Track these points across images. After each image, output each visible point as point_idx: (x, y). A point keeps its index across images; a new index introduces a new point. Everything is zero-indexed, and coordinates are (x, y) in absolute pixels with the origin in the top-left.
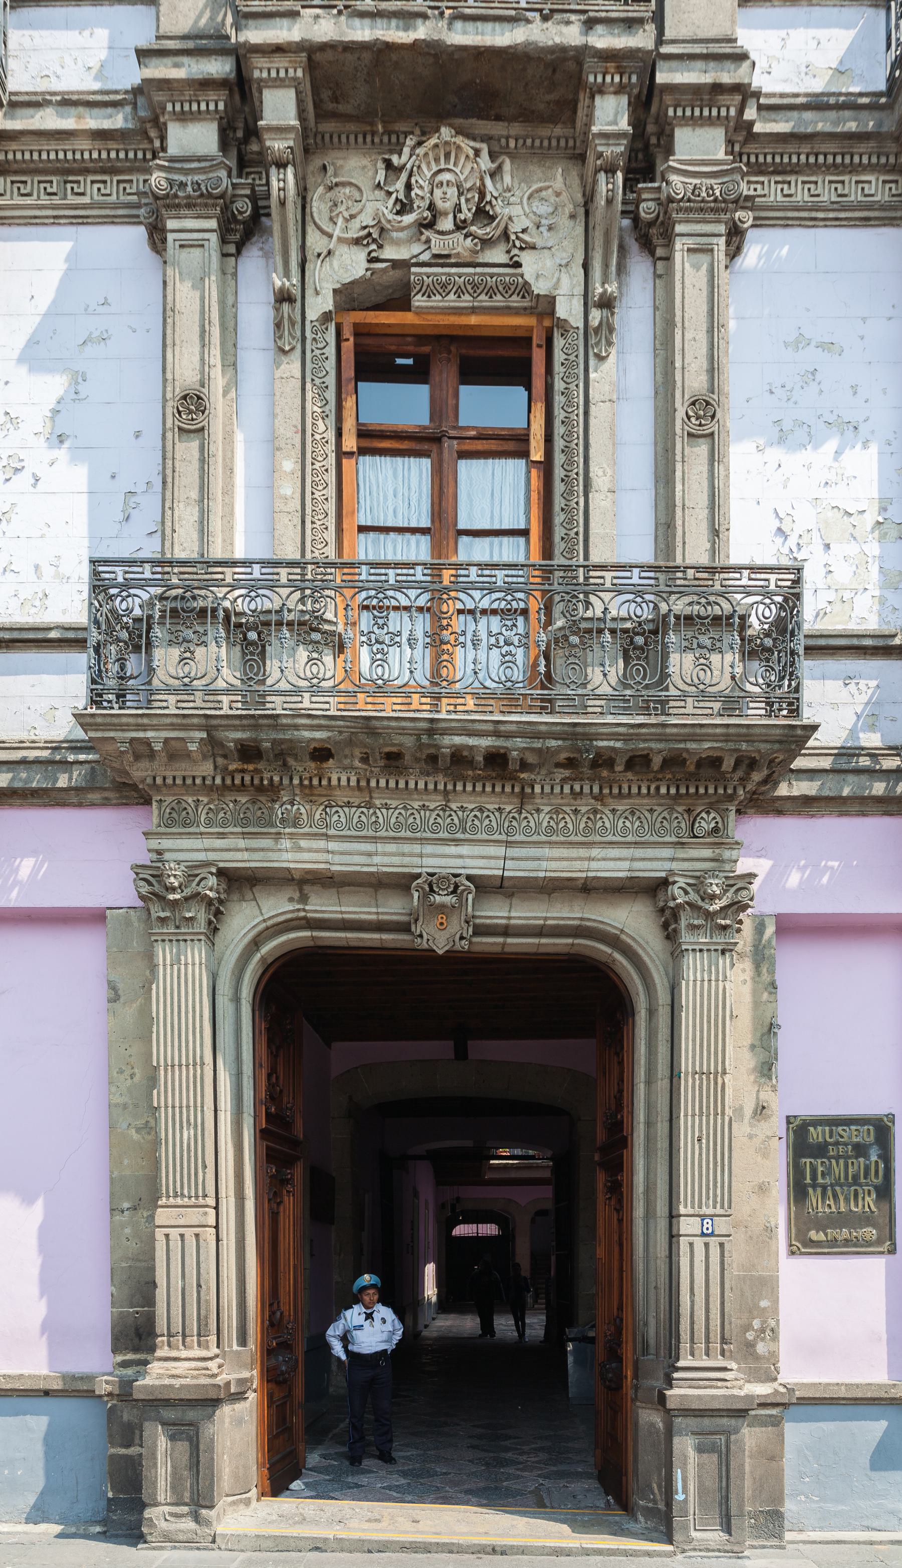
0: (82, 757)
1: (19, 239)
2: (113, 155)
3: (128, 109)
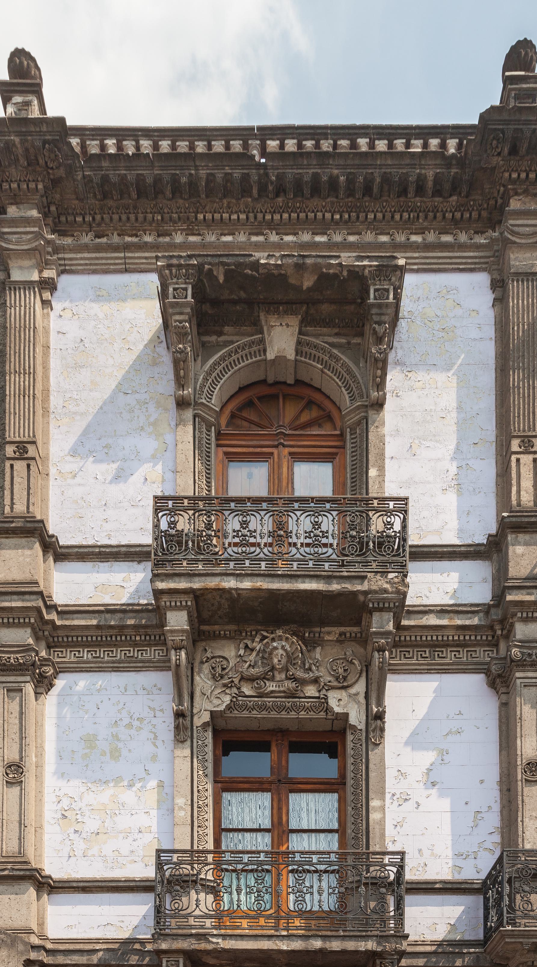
0: (472, 950)
1: (404, 681)
2: (467, 638)
3: (481, 614)
